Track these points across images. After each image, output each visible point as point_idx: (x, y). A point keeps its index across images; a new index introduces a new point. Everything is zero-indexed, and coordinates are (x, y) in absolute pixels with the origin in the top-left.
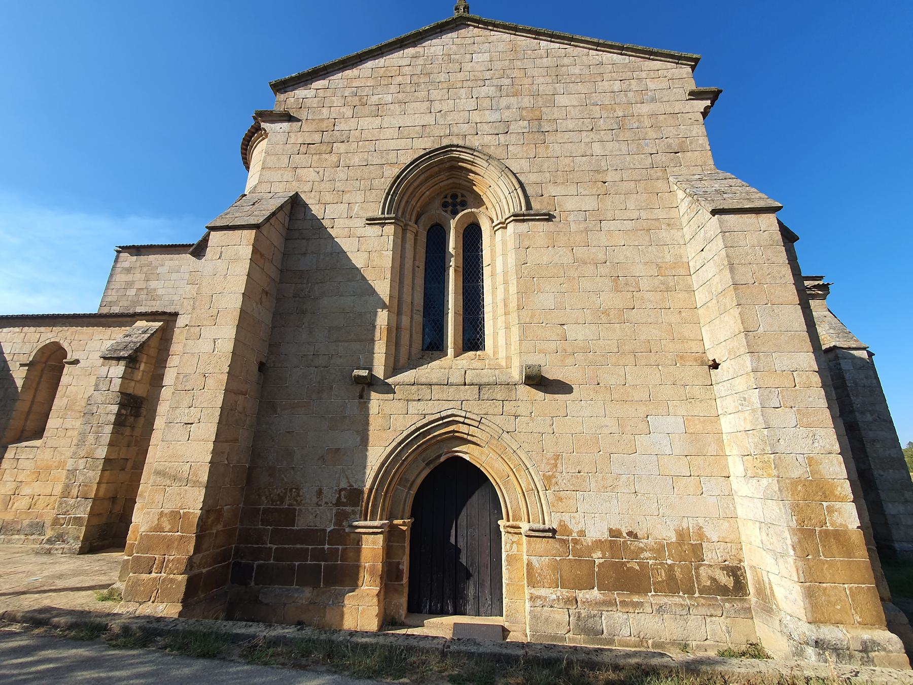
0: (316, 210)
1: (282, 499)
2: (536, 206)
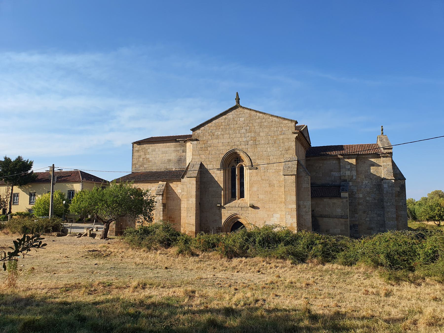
0: (206, 166)
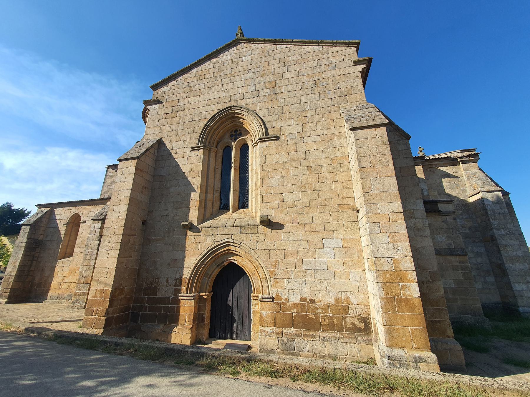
0: (168, 146)
1: (152, 284)
2: (271, 133)
